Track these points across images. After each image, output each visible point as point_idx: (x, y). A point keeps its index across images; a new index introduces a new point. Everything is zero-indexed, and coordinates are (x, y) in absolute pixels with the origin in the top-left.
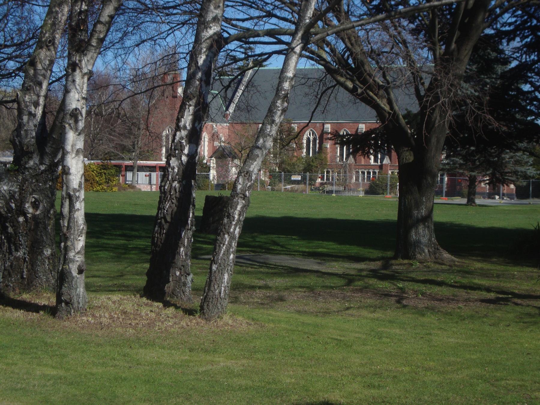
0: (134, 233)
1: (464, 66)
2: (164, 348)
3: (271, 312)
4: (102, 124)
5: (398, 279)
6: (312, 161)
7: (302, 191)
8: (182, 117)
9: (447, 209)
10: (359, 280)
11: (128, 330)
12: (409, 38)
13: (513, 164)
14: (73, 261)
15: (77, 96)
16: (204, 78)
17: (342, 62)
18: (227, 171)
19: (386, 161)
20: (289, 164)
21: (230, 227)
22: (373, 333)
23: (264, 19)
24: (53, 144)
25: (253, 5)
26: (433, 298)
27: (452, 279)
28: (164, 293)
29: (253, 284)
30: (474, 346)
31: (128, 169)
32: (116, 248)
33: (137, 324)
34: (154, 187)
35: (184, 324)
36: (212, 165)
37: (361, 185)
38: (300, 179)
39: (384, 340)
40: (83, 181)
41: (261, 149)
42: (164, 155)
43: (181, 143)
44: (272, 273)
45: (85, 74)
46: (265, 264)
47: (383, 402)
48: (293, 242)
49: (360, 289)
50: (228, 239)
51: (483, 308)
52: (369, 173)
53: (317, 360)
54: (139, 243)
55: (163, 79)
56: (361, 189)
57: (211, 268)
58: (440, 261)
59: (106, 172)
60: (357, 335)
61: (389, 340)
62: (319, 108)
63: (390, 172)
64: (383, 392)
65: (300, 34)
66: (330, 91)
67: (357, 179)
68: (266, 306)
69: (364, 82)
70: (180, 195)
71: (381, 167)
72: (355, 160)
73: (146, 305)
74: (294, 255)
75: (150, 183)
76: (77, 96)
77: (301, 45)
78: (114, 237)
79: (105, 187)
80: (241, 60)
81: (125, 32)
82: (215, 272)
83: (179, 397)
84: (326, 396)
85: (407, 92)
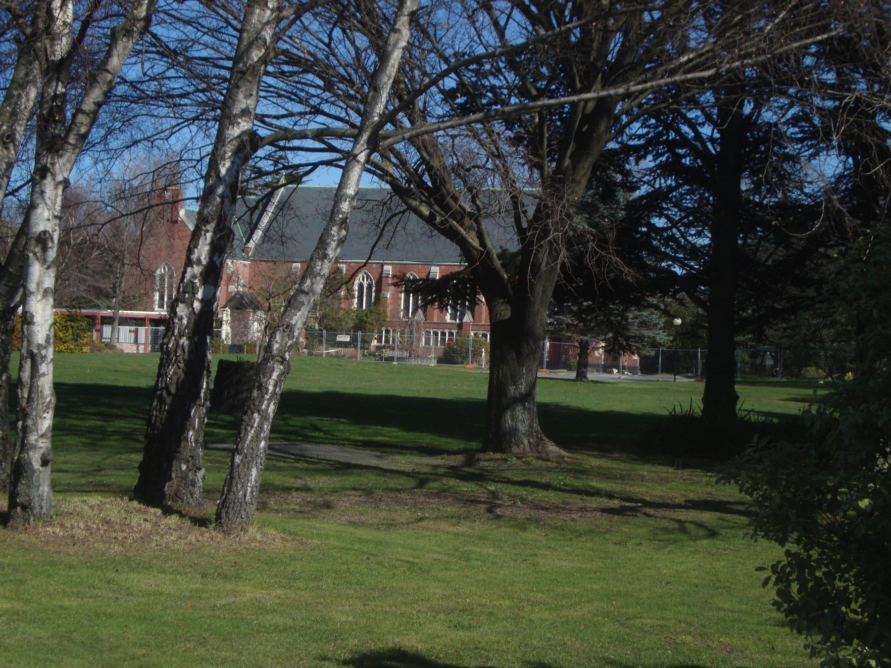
0: (114, 411)
1: (578, 191)
2: (164, 572)
3: (314, 523)
4: (70, 258)
5: (489, 480)
6: (366, 315)
7: (351, 357)
8: (196, 246)
9: (555, 386)
10: (435, 480)
11: (112, 546)
12: (505, 148)
13: (638, 326)
14: (34, 447)
15: (46, 214)
16: (228, 193)
17: (414, 177)
18: (247, 327)
19: (468, 318)
20: (333, 319)
21: (261, 402)
22: (457, 554)
23: (308, 117)
24: (8, 281)
25: (293, 97)
26: (536, 506)
27: (561, 481)
28: (163, 495)
29: (287, 485)
30: (596, 572)
31: (106, 321)
32: (89, 432)
33: (126, 538)
34: (141, 348)
35: (193, 539)
36: (225, 319)
37: (433, 350)
38: (348, 340)
39: (473, 562)
40: (52, 334)
41: (307, 293)
42: (157, 303)
43: (193, 283)
44: (314, 470)
45: (60, 183)
46: (302, 458)
47: (477, 648)
48: (342, 427)
49: (437, 493)
50: (257, 420)
51: (604, 520)
52: (443, 334)
53: (382, 590)
54: (122, 425)
55: (160, 196)
56: (433, 355)
57: (232, 461)
58: (543, 455)
59: (75, 324)
60: (436, 556)
61: (479, 563)
62: (381, 243)
63: (472, 334)
64: (475, 635)
65: (365, 137)
66: (396, 219)
67: (427, 342)
68: (306, 515)
69: (446, 208)
70: (189, 355)
71: (460, 326)
72: (425, 316)
73: (139, 511)
74: (344, 445)
75: (136, 341)
76: (46, 214)
77: (367, 151)
78: (85, 416)
79: (72, 347)
80: (268, 173)
81: (109, 128)
82: (238, 466)
83: (189, 641)
84: (397, 640)
85: (503, 224)
